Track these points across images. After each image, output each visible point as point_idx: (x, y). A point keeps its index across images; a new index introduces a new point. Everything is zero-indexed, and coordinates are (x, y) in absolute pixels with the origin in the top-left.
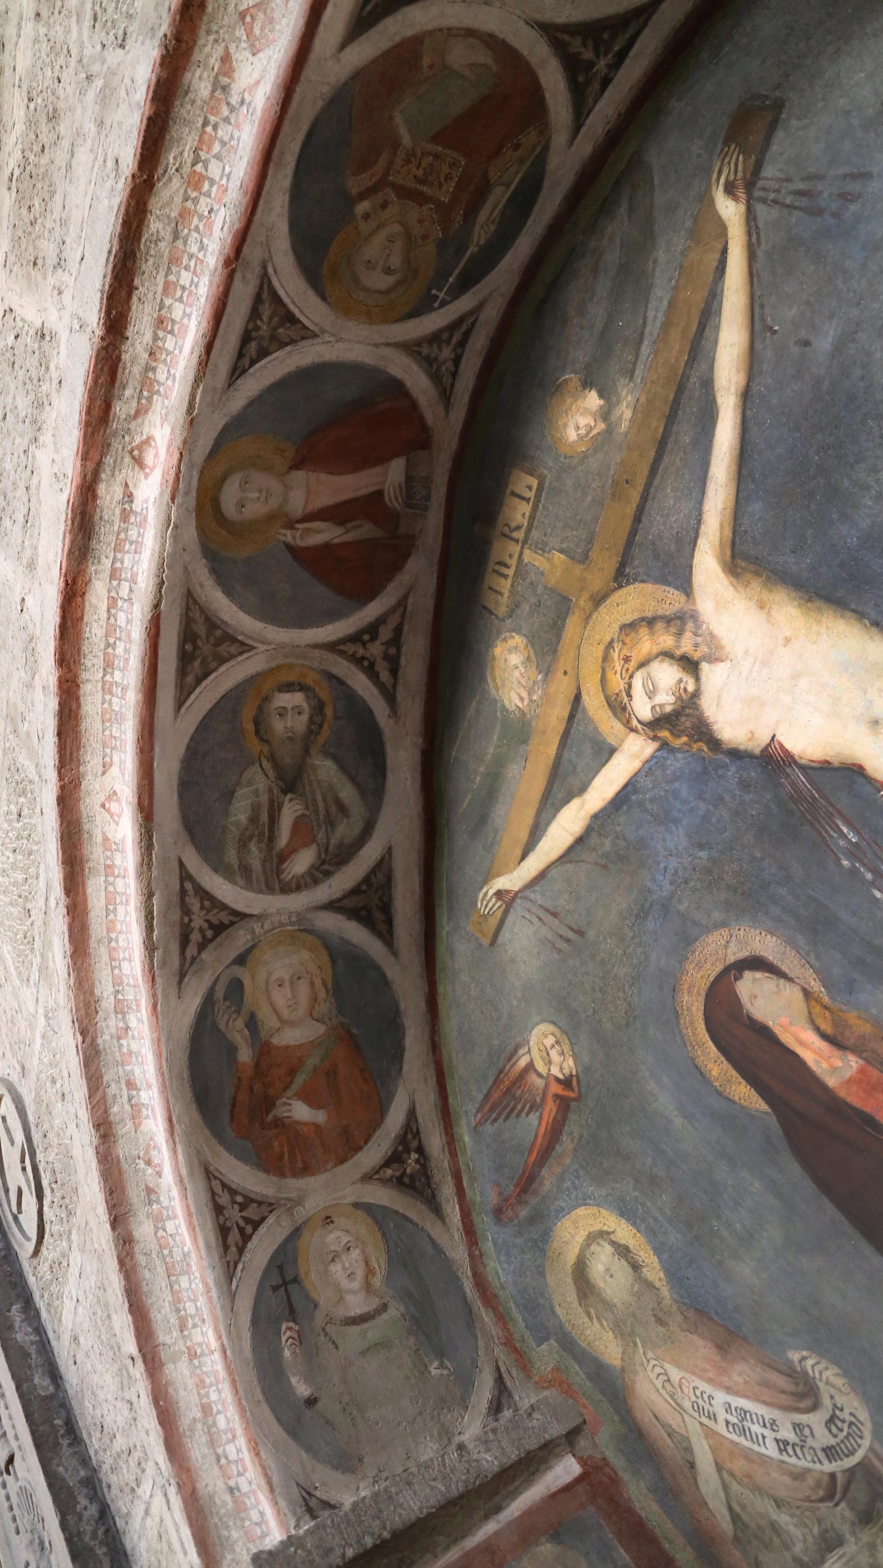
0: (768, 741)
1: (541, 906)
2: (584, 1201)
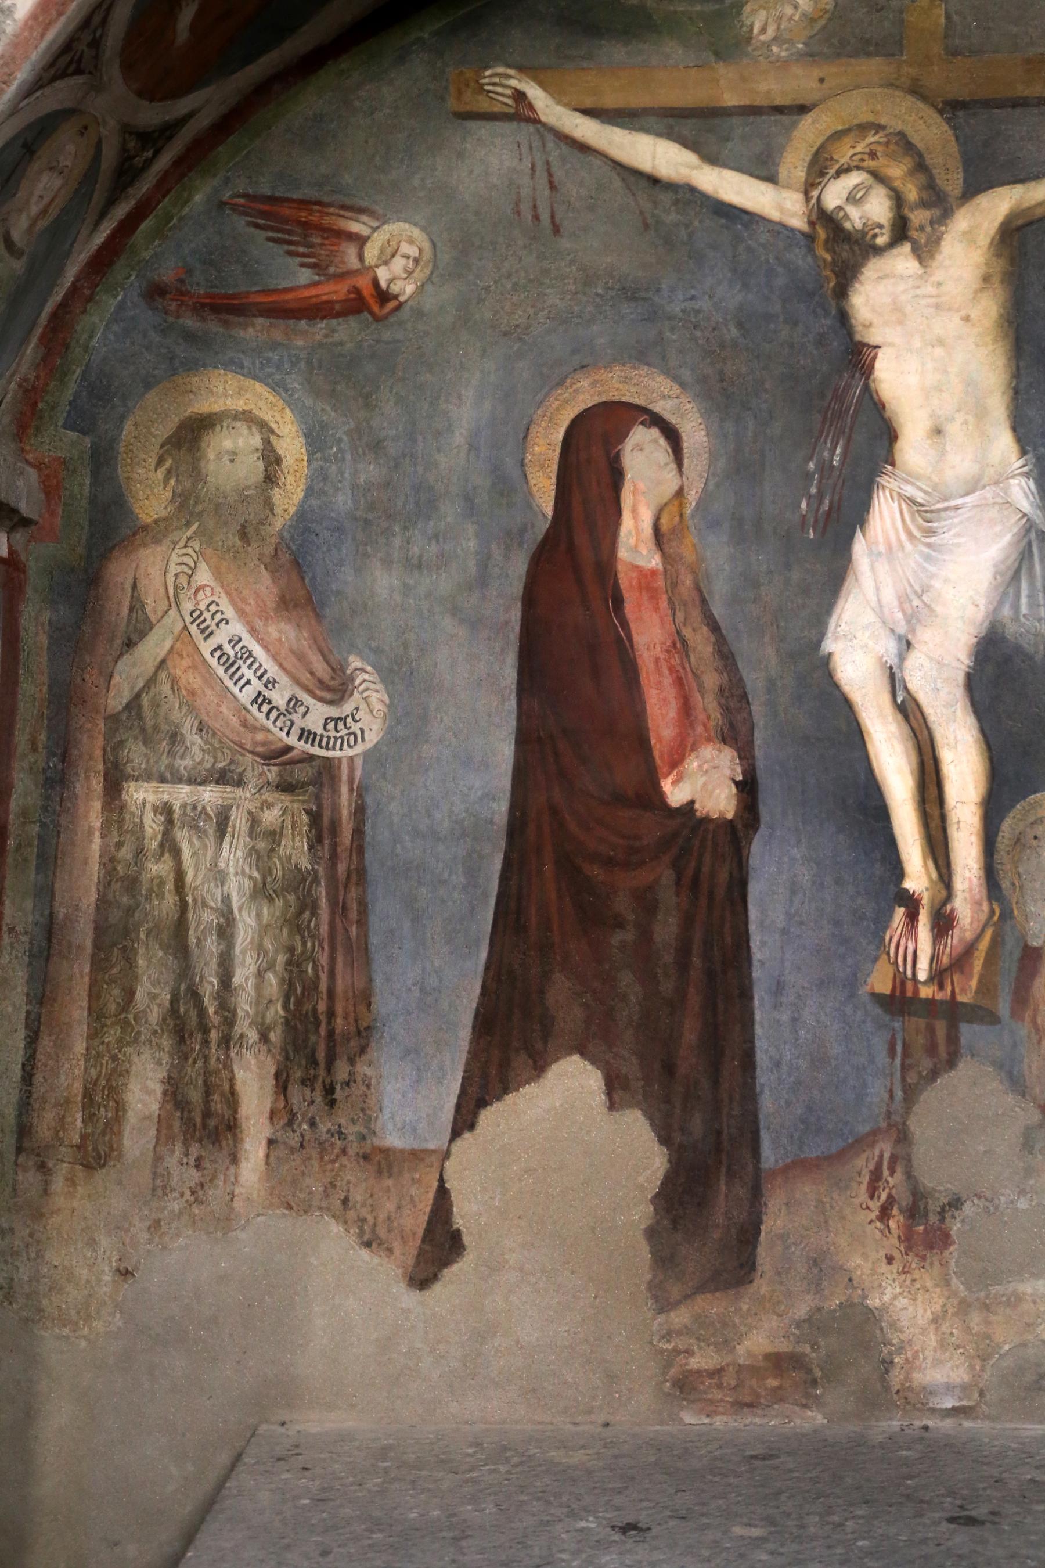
0: (871, 343)
1: (548, 163)
2: (278, 387)
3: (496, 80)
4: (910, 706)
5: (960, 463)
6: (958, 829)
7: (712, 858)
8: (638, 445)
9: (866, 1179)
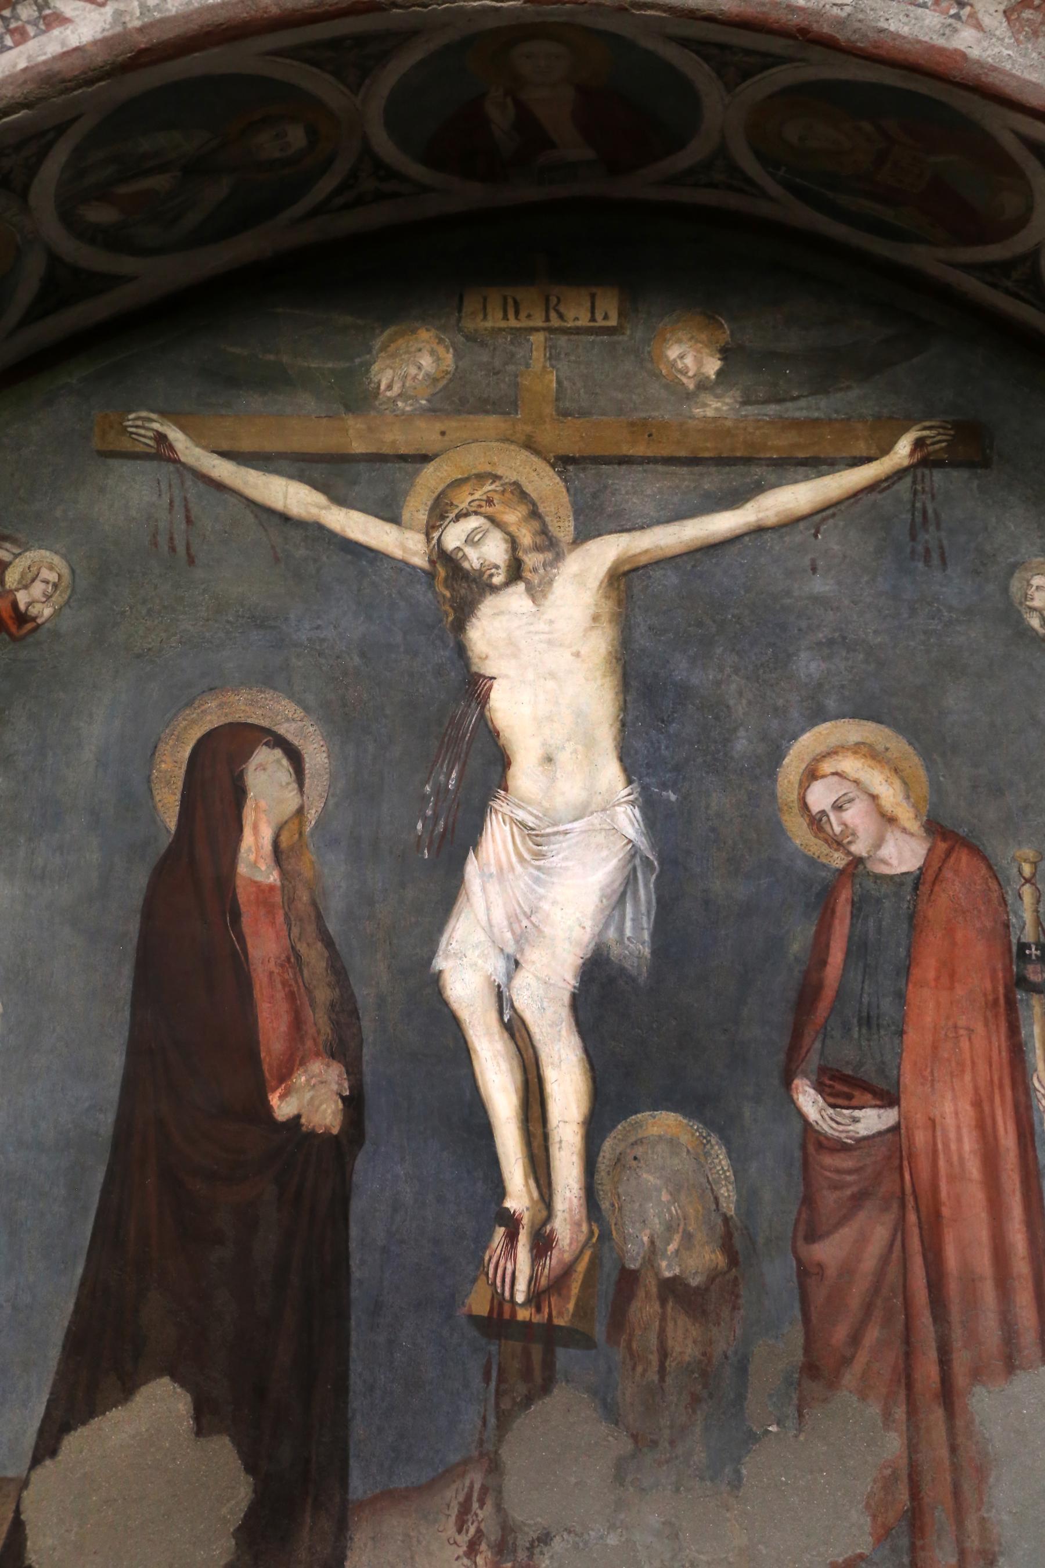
0: (487, 675)
1: (185, 499)
3: (139, 423)
4: (517, 1024)
5: (570, 789)
6: (560, 1148)
7: (318, 1167)
8: (261, 765)
9: (454, 1511)
